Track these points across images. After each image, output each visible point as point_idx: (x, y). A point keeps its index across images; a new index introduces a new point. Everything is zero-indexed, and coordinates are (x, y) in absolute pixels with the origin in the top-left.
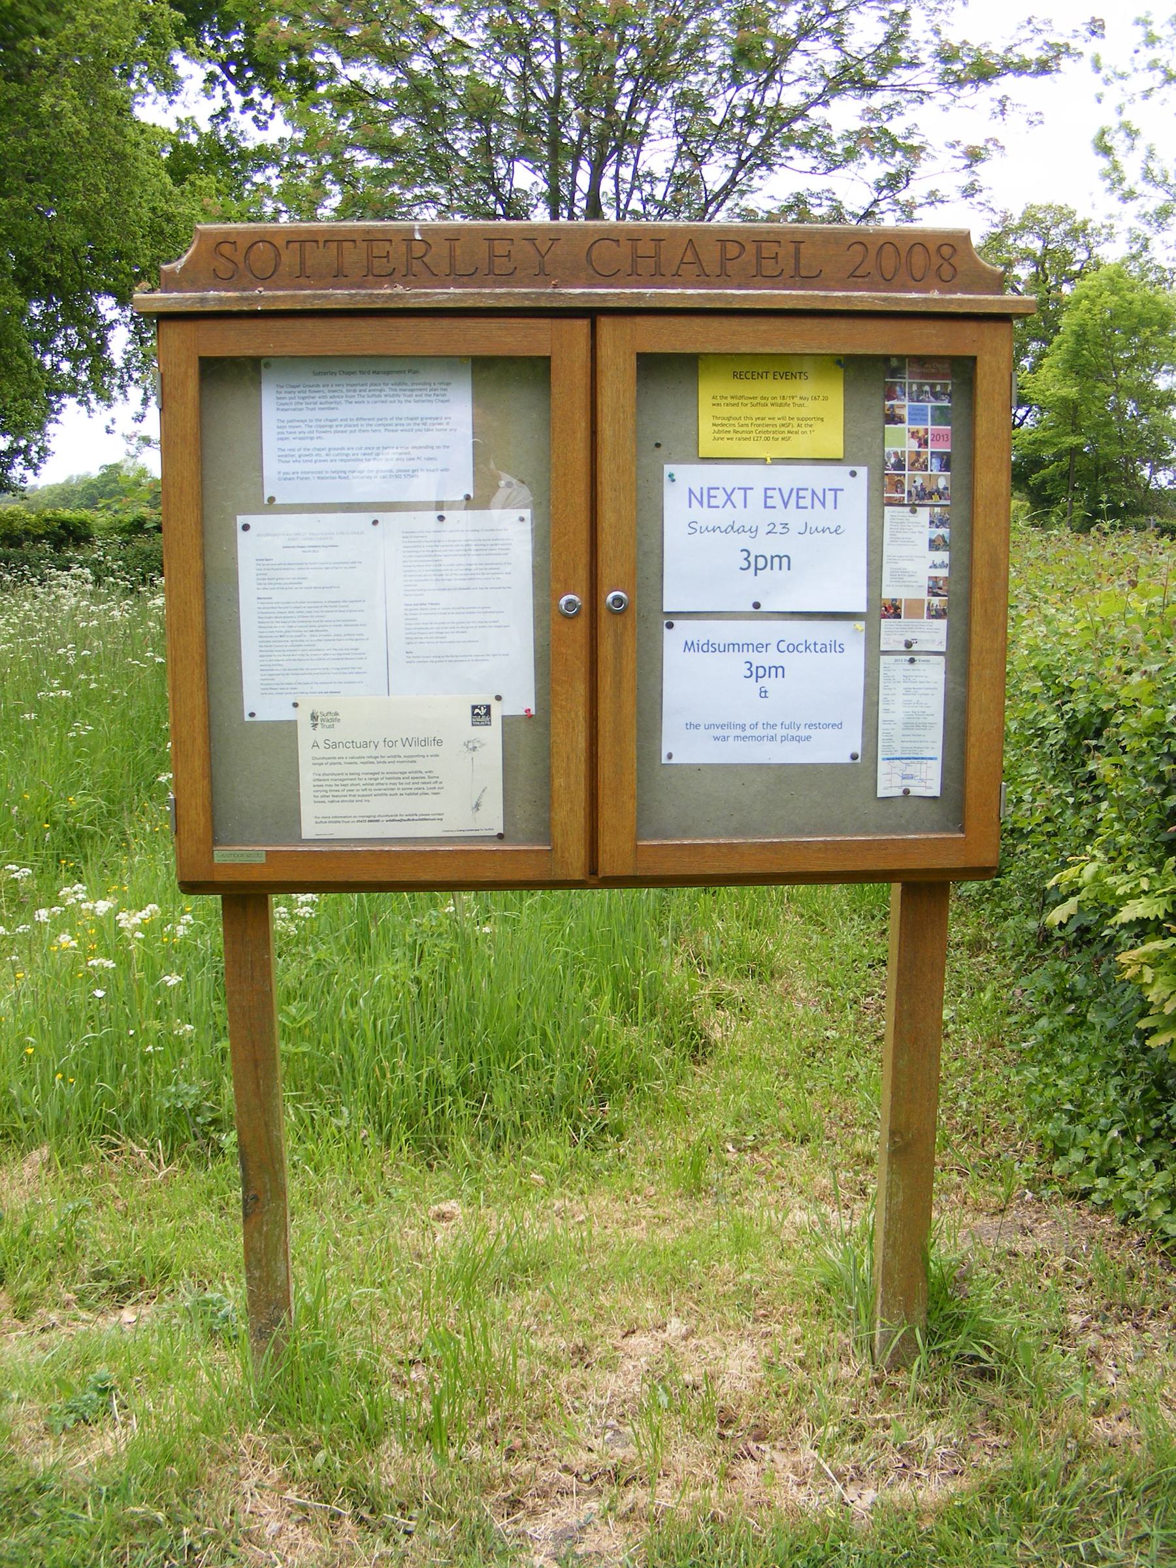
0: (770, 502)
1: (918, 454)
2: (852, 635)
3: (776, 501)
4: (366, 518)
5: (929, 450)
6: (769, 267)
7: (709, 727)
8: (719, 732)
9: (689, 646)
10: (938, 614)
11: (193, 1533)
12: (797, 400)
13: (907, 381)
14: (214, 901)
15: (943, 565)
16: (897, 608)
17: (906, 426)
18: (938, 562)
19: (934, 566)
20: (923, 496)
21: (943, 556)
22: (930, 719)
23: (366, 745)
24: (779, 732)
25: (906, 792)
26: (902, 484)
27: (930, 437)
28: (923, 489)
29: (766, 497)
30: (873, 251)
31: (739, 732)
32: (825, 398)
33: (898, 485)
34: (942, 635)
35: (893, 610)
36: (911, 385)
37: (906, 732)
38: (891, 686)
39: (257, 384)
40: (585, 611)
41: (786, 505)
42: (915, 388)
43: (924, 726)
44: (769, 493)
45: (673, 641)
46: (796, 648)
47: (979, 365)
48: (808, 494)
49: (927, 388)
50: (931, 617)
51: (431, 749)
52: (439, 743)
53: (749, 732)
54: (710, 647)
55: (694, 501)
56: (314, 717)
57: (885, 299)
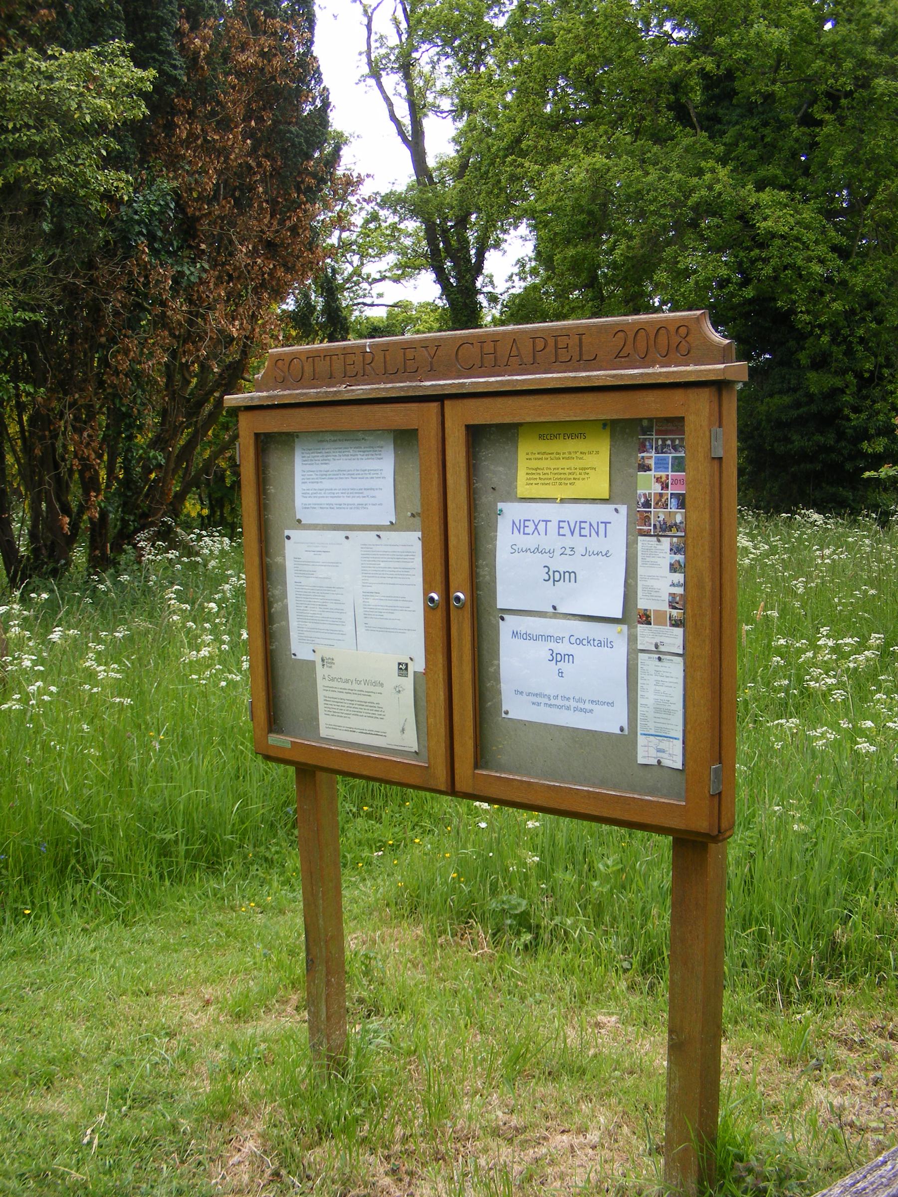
0: (562, 531)
1: (661, 495)
2: (617, 635)
3: (565, 531)
4: (342, 534)
5: (670, 492)
6: (564, 356)
7: (529, 694)
8: (535, 699)
9: (515, 634)
10: (676, 624)
11: (197, 1145)
12: (578, 455)
13: (654, 437)
14: (291, 770)
15: (678, 585)
16: (648, 617)
17: (652, 473)
18: (676, 582)
19: (673, 585)
20: (664, 529)
21: (679, 577)
22: (673, 707)
23: (347, 681)
24: (573, 704)
25: (659, 762)
26: (649, 519)
27: (670, 481)
28: (665, 523)
29: (559, 528)
30: (631, 335)
31: (546, 700)
32: (597, 453)
33: (646, 520)
34: (680, 641)
35: (646, 618)
36: (657, 440)
37: (658, 715)
38: (646, 677)
39: (293, 449)
40: (443, 605)
41: (572, 534)
42: (660, 442)
43: (669, 712)
44: (562, 524)
45: (507, 627)
46: (581, 642)
47: (686, 423)
48: (586, 526)
49: (669, 442)
50: (673, 625)
51: (378, 689)
52: (382, 685)
53: (553, 702)
54: (527, 636)
55: (515, 530)
56: (323, 660)
57: (614, 376)
